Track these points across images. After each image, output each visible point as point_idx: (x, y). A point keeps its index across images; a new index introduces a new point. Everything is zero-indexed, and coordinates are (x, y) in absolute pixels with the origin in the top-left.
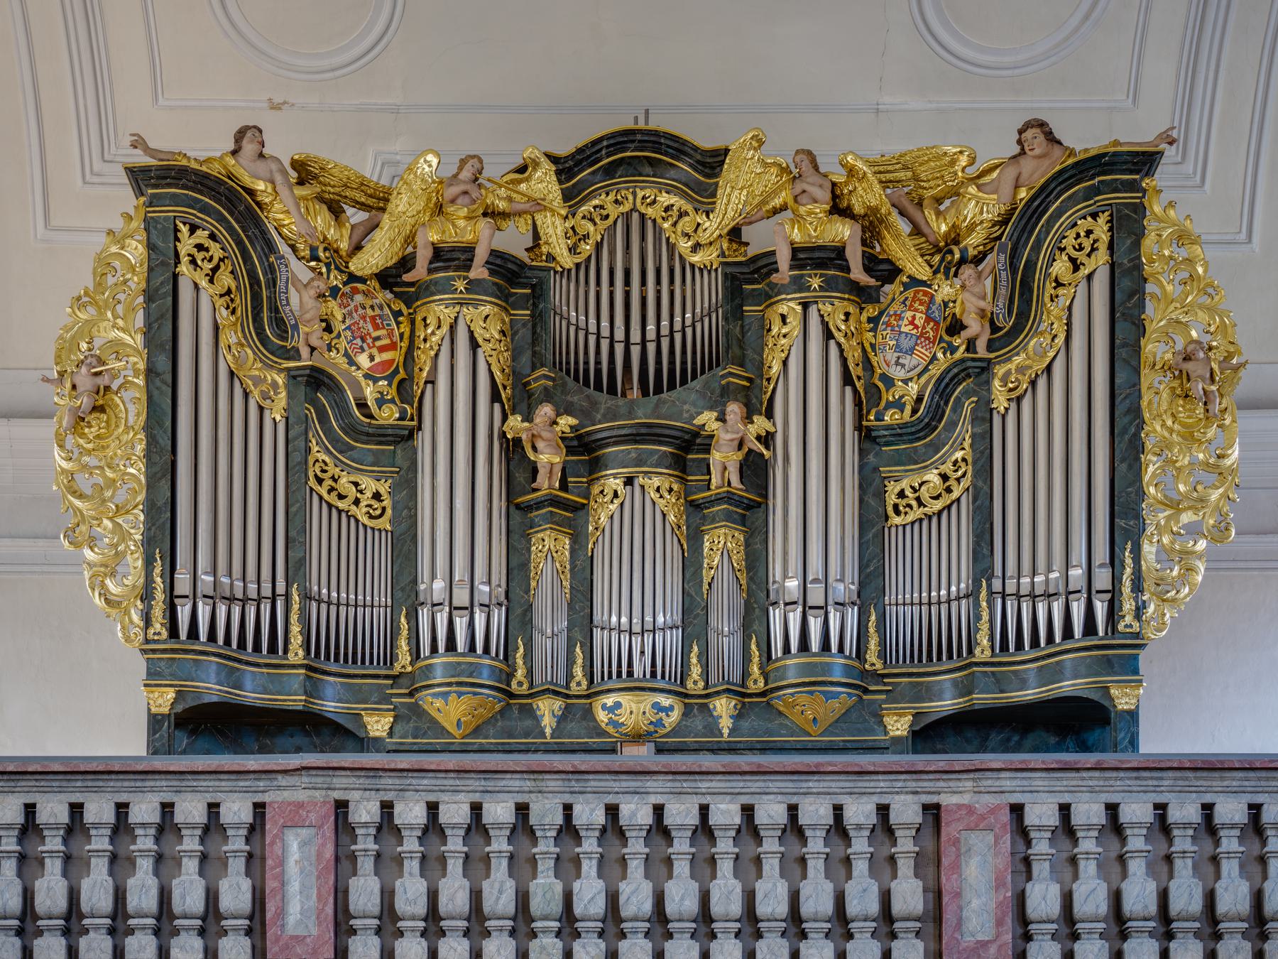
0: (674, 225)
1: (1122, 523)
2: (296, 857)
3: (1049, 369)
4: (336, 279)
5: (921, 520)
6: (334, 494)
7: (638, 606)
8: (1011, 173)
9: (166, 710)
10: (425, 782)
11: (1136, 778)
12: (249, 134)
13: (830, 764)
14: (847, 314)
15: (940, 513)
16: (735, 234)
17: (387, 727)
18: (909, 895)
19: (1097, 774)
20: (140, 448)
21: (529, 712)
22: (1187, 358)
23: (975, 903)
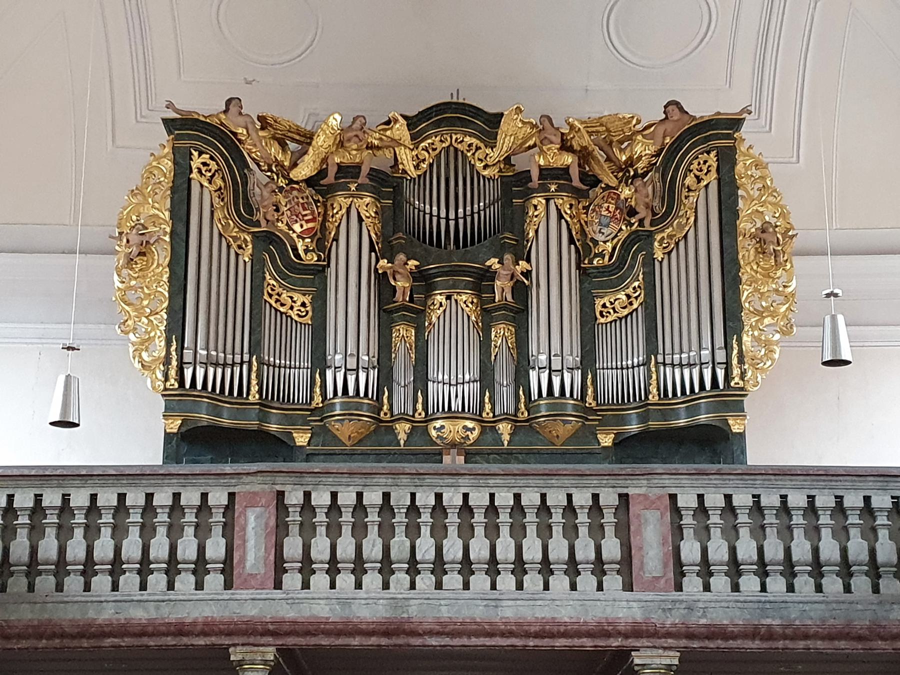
0: (474, 154)
1: (731, 324)
2: (253, 525)
3: (685, 237)
4: (282, 182)
5: (615, 321)
6: (278, 303)
7: (453, 376)
8: (661, 130)
9: (175, 431)
10: (331, 480)
11: (741, 480)
12: (233, 102)
13: (565, 469)
14: (571, 205)
15: (626, 316)
16: (507, 160)
17: (307, 440)
18: (216, 548)
19: (718, 477)
20: (165, 277)
21: (391, 431)
22: (763, 232)
23: (652, 553)
